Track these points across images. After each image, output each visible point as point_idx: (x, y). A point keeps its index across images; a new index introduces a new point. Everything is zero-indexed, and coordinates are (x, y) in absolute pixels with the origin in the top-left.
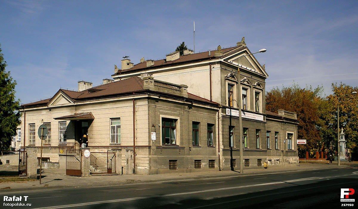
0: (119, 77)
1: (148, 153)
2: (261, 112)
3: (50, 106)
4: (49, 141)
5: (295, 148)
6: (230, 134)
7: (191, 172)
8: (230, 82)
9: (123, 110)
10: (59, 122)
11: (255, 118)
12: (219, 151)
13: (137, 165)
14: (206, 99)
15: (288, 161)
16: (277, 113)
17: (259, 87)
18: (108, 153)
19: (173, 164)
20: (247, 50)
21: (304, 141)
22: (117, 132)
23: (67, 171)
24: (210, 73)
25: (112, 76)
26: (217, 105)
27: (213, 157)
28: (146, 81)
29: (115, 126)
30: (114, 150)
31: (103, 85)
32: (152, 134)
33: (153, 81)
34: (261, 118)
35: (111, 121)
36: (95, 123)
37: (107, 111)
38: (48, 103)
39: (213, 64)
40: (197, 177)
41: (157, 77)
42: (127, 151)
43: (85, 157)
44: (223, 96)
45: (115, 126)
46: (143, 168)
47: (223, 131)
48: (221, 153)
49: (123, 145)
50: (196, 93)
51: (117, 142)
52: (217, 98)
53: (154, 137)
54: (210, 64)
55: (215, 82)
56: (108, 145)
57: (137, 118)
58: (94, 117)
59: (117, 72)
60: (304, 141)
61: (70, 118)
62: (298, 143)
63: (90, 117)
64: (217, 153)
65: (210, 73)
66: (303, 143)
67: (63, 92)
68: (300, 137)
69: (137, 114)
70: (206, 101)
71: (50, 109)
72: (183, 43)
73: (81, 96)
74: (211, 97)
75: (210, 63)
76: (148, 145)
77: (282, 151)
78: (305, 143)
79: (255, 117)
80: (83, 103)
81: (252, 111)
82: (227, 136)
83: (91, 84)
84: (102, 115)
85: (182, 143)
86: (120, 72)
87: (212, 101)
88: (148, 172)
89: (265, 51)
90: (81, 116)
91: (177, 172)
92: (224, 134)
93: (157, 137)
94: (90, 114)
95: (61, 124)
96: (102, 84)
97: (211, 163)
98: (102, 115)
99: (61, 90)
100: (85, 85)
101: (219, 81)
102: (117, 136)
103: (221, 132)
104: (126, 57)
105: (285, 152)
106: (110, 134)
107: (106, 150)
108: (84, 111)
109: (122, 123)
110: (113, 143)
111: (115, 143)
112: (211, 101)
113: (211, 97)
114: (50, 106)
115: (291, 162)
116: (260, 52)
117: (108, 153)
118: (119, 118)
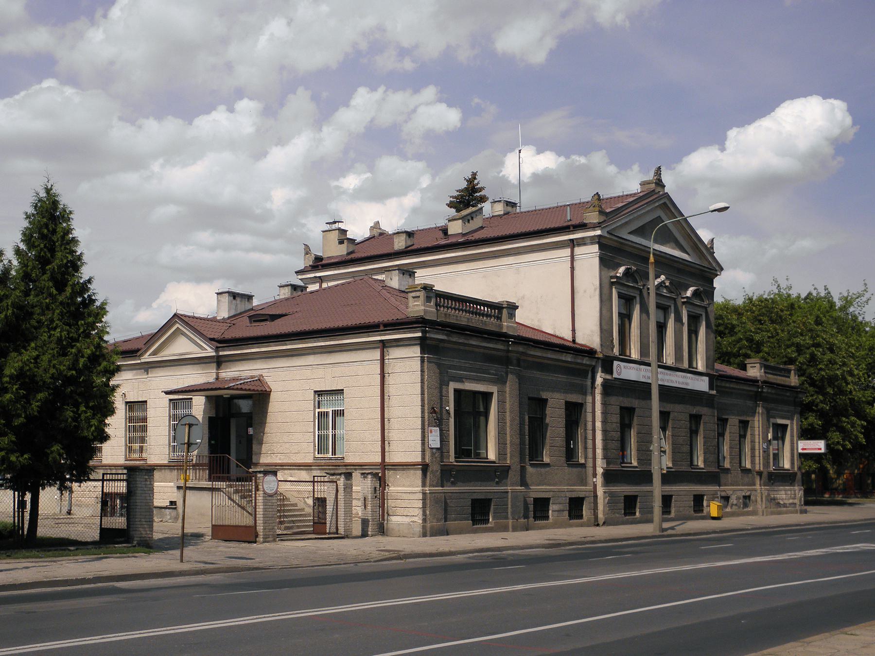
0: (316, 277)
1: (420, 482)
2: (701, 366)
3: (146, 358)
4: (141, 449)
5: (792, 463)
6: (625, 427)
7: (527, 530)
8: (624, 291)
9: (353, 372)
10: (170, 400)
11: (687, 384)
12: (595, 475)
13: (390, 513)
14: (557, 337)
15: (774, 499)
16: (744, 367)
17: (697, 302)
18: (314, 482)
19: (479, 513)
20: (668, 202)
21: (818, 446)
22: (334, 427)
23: (214, 527)
24: (572, 268)
25: (296, 272)
26: (590, 352)
27: (579, 490)
28: (414, 294)
29: (330, 410)
30: (333, 475)
31: (281, 301)
32: (431, 432)
33: (432, 295)
34: (702, 385)
35: (317, 399)
36: (275, 406)
37: (307, 373)
38: (138, 350)
39: (579, 245)
40: (547, 542)
41: (423, 276)
42: (365, 477)
43: (265, 493)
44: (605, 327)
45: (330, 410)
46: (407, 520)
47: (604, 422)
48: (599, 480)
49: (351, 459)
50: (532, 320)
51: (334, 453)
52: (589, 334)
53: (434, 440)
54: (573, 244)
55: (585, 292)
56: (309, 460)
57: (391, 390)
58: (269, 387)
59: (311, 263)
60: (818, 446)
61: (204, 390)
62: (800, 451)
63: (260, 389)
64: (591, 480)
65: (572, 268)
66: (815, 449)
67: (187, 324)
68: (808, 434)
69: (389, 380)
70: (562, 342)
71: (148, 367)
72: (474, 175)
73: (230, 330)
74: (574, 330)
75: (572, 240)
76: (419, 460)
77: (760, 474)
78: (823, 451)
79: (689, 381)
80: (239, 352)
81: (679, 366)
82: (614, 434)
83: (249, 298)
84: (291, 384)
85: (501, 453)
86: (319, 263)
87: (578, 340)
88: (418, 529)
89: (726, 208)
90: (239, 387)
91: (491, 530)
92: (608, 429)
93: (443, 439)
94: (260, 380)
95: (175, 407)
96: (277, 298)
97: (575, 507)
98: (291, 384)
99: (175, 315)
100: (234, 302)
101: (595, 290)
102: (334, 436)
103: (598, 424)
104: (335, 222)
105: (765, 475)
106: (314, 432)
107: (304, 475)
108: (240, 372)
109: (348, 404)
110: (322, 456)
111: (330, 455)
112: (574, 341)
113: (574, 330)
114: (146, 358)
115: (782, 502)
116: (712, 211)
117: (314, 482)
118: (340, 392)
